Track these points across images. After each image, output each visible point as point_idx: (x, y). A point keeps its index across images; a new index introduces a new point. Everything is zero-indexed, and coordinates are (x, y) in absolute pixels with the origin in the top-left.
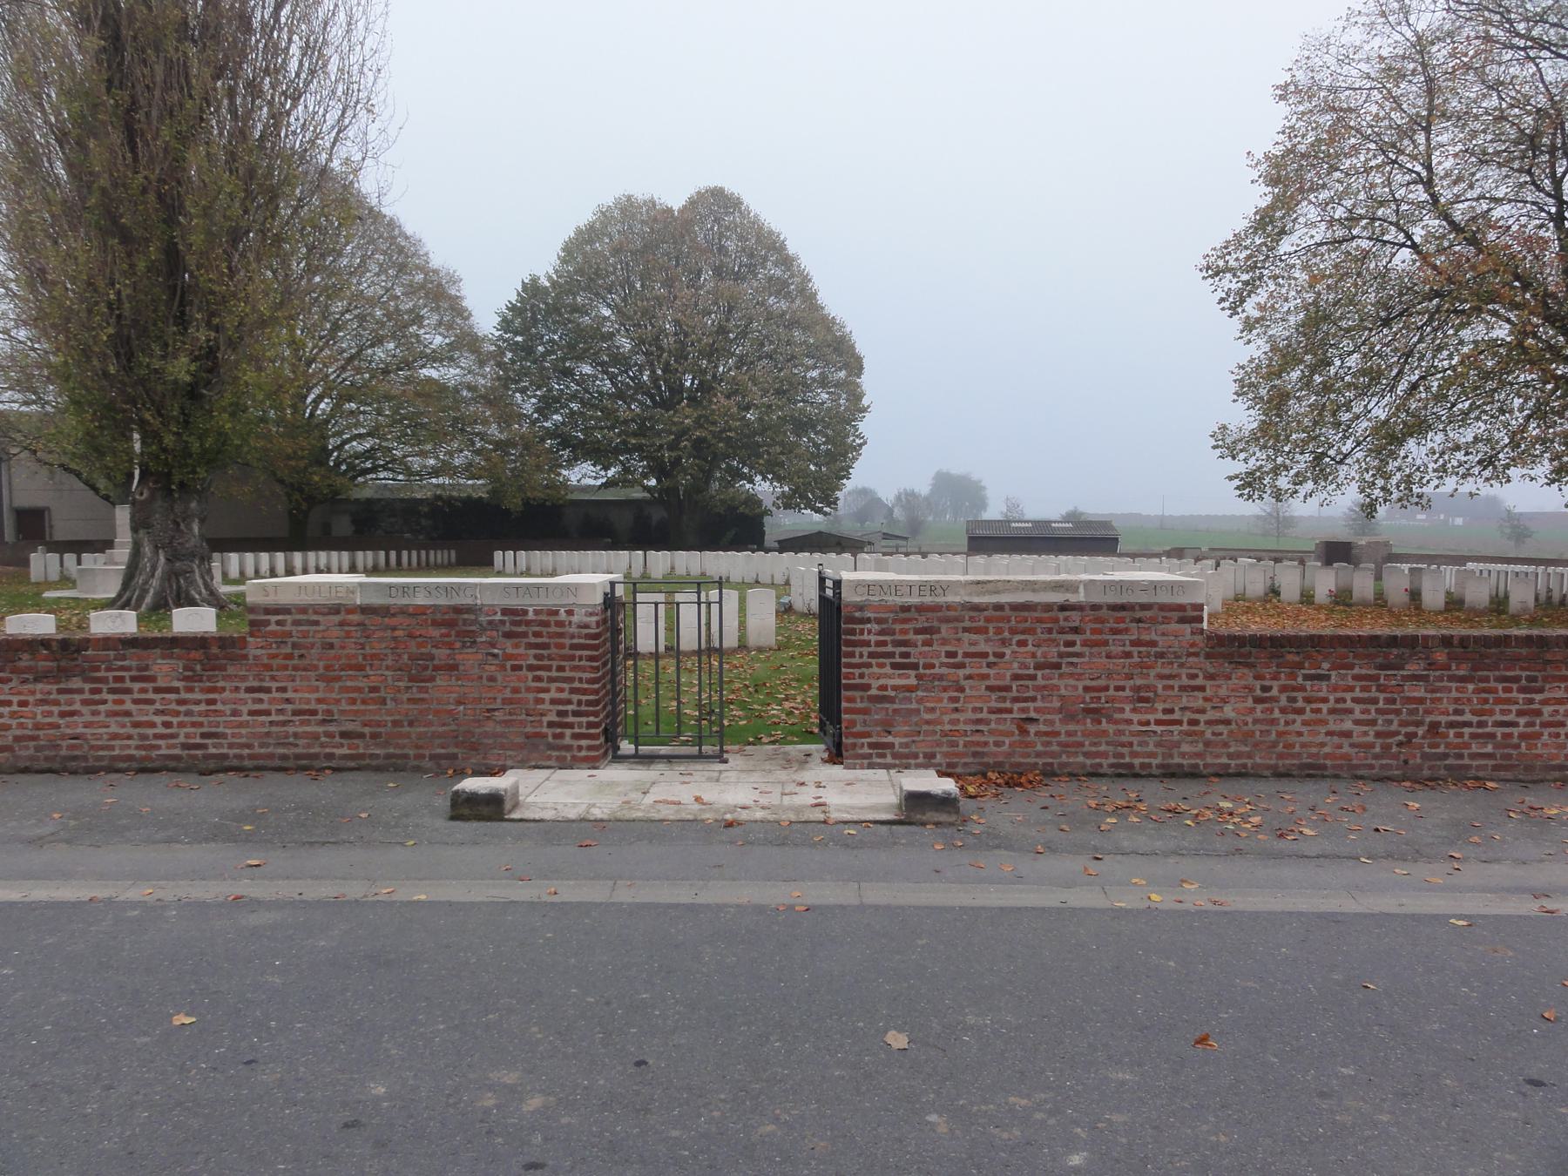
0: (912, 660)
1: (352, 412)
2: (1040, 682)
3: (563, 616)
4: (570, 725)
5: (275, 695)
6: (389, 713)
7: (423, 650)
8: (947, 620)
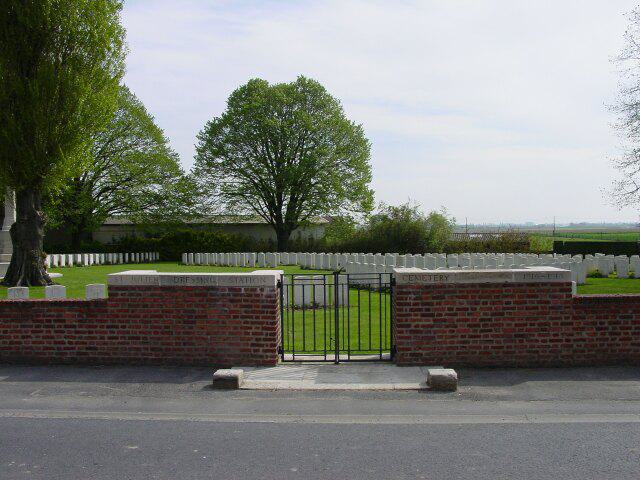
1: (157, 197)
3: (259, 292)
4: (262, 346)
8: (449, 292)
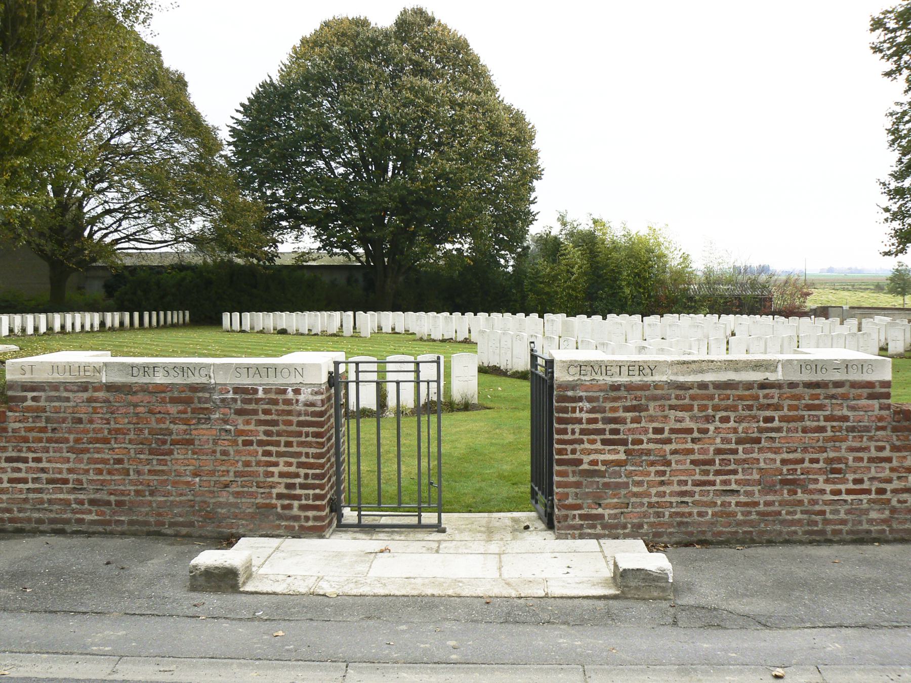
0: (621, 436)
2: (741, 455)
3: (290, 395)
5: (31, 464)
6: (131, 482)
7: (163, 426)
8: (655, 398)
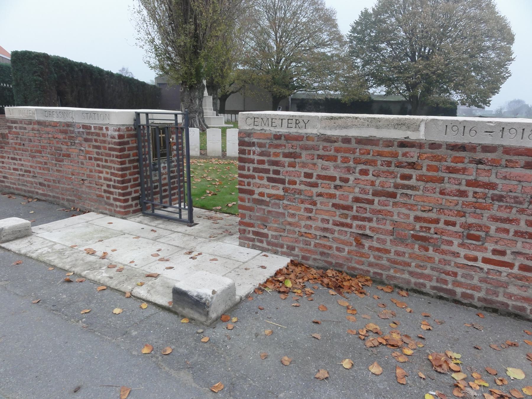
3: (104, 131)
